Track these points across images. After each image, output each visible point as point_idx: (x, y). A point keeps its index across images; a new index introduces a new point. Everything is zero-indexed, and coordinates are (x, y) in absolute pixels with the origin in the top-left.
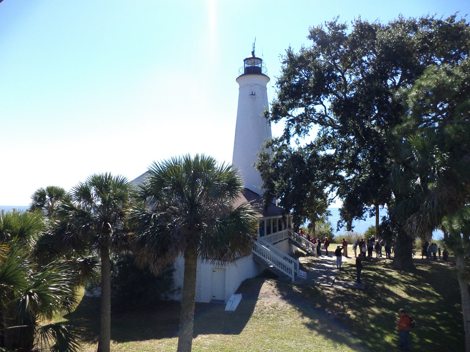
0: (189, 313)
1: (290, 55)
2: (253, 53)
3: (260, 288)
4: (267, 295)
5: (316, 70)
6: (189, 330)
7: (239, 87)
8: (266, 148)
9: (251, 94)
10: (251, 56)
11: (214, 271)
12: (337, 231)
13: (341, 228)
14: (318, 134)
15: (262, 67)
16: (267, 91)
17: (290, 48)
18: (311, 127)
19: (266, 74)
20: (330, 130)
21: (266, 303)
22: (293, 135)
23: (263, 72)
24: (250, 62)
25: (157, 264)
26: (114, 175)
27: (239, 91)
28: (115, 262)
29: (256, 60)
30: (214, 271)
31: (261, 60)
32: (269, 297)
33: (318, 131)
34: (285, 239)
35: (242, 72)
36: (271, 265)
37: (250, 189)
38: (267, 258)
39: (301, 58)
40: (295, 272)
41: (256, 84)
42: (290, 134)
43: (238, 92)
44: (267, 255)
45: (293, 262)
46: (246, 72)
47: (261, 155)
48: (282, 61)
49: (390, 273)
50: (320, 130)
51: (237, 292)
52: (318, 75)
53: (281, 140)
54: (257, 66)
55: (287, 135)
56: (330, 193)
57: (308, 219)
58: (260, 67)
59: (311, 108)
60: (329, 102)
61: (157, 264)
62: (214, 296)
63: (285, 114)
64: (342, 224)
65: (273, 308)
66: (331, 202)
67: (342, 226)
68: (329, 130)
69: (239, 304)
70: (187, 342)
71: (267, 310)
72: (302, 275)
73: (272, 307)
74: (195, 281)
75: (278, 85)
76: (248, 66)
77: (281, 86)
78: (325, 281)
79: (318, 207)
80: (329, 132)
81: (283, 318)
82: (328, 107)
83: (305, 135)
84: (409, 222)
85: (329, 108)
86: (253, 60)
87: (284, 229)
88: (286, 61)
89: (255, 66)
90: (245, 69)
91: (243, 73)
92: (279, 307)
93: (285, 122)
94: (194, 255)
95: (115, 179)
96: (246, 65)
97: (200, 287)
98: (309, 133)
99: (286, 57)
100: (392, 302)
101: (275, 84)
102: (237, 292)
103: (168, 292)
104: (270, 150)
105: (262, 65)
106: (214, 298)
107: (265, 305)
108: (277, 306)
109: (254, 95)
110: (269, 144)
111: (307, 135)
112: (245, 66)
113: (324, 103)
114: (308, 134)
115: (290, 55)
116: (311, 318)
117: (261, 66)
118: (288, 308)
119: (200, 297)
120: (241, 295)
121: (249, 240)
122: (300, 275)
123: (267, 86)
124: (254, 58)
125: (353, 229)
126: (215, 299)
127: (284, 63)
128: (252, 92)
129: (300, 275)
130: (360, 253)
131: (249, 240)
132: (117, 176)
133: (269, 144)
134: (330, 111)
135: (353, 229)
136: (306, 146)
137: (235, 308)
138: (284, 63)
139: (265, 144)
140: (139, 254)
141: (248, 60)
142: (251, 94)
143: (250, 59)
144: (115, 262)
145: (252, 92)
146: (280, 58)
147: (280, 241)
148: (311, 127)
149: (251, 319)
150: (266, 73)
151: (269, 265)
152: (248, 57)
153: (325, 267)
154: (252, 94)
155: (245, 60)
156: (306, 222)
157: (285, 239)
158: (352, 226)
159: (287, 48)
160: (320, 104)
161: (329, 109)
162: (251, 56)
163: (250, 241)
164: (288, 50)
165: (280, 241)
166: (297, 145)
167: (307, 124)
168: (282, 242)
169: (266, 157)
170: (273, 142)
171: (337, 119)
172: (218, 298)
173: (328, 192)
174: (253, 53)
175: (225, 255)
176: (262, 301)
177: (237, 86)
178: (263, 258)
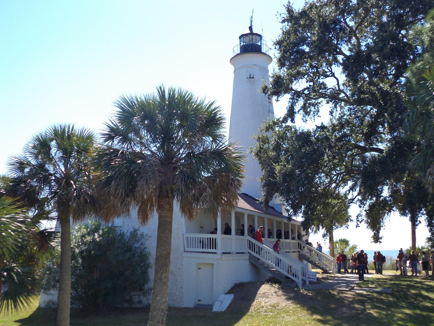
0: (164, 275)
1: (290, 10)
2: (251, 28)
3: (258, 288)
4: (265, 295)
5: (320, 20)
6: (163, 295)
8: (266, 131)
9: (249, 78)
10: (249, 32)
11: (199, 268)
12: (356, 227)
13: (361, 222)
14: (330, 113)
15: (262, 44)
17: (289, 3)
18: (321, 103)
19: (267, 53)
20: (346, 111)
21: (263, 303)
22: (299, 111)
23: (264, 50)
24: (247, 39)
25: (125, 205)
26: (78, 129)
27: (233, 75)
28: (77, 251)
29: (254, 36)
30: (199, 268)
31: (260, 36)
32: (268, 297)
33: (330, 110)
35: (238, 50)
37: (249, 195)
38: (266, 259)
39: (304, 14)
40: (302, 280)
41: (255, 65)
42: (295, 111)
43: (233, 75)
46: (243, 51)
47: (259, 138)
48: (281, 20)
49: (427, 283)
50: (332, 109)
51: (229, 292)
52: (322, 26)
53: (285, 120)
55: (291, 113)
56: (349, 192)
57: (323, 228)
59: (320, 82)
60: (342, 74)
61: (125, 205)
62: (199, 300)
63: (288, 90)
64: (361, 219)
65: (273, 307)
66: (352, 203)
67: (362, 221)
68: (345, 112)
69: (231, 304)
70: (161, 310)
71: (265, 308)
72: (310, 277)
73: (270, 306)
74: (170, 242)
75: (277, 47)
77: (280, 48)
79: (335, 210)
80: (345, 115)
81: (284, 316)
82: (341, 83)
83: (315, 117)
84: (430, 174)
85: (343, 83)
86: (251, 36)
88: (285, 19)
90: (241, 48)
91: (239, 52)
92: (280, 306)
93: (289, 100)
94: (169, 206)
95: (79, 134)
97: (182, 288)
98: (319, 114)
99: (285, 15)
100: (409, 263)
101: (273, 45)
102: (229, 292)
103: (142, 292)
104: (269, 134)
105: (262, 42)
107: (263, 304)
108: (278, 306)
109: (253, 78)
110: (269, 125)
111: (317, 116)
112: (240, 44)
113: (336, 75)
114: (318, 115)
115: (290, 10)
117: (261, 43)
118: (291, 308)
119: (182, 300)
121: (233, 182)
122: (308, 277)
123: (269, 68)
124: (252, 33)
125: (381, 240)
126: (202, 303)
127: (284, 21)
128: (250, 75)
129: (309, 278)
131: (233, 182)
132: (81, 129)
133: (269, 125)
134: (345, 86)
135: (381, 240)
136: (315, 128)
138: (284, 21)
139: (263, 126)
140: (105, 207)
142: (249, 77)
143: (246, 35)
144: (77, 251)
145: (250, 75)
146: (278, 16)
148: (321, 103)
149: (245, 318)
152: (245, 33)
153: (345, 280)
154: (250, 78)
155: (240, 37)
156: (320, 230)
158: (380, 236)
159: (286, 3)
160: (331, 76)
161: (343, 85)
162: (249, 32)
163: (234, 183)
164: (287, 5)
166: (304, 122)
168: (290, 253)
169: (265, 140)
170: (275, 123)
171: (350, 87)
172: (204, 302)
173: (348, 192)
174: (251, 28)
175: (204, 194)
176: (258, 302)
177: (232, 68)
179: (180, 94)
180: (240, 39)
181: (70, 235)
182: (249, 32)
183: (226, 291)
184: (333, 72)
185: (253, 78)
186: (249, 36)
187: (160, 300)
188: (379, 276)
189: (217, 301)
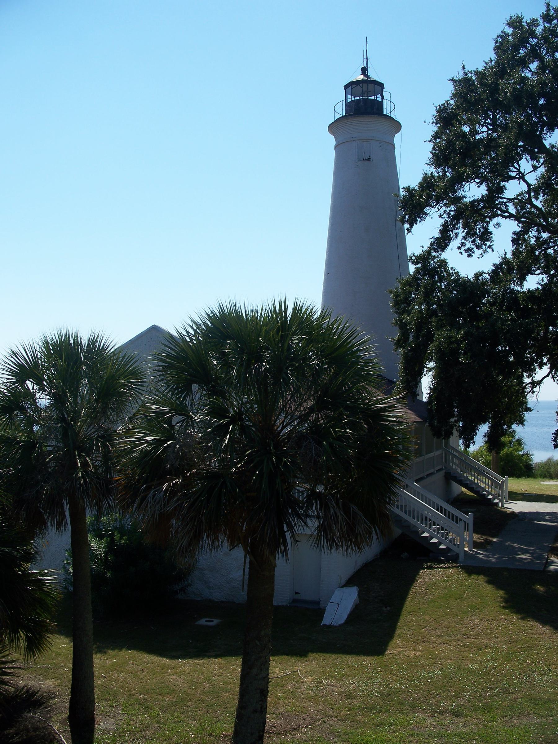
2: (364, 70)
7: (334, 143)
16: (395, 150)
19: (393, 116)
27: (334, 152)
29: (371, 86)
31: (381, 85)
34: (438, 471)
35: (342, 111)
36: (424, 532)
38: (414, 518)
43: (332, 154)
44: (414, 511)
45: (461, 520)
51: (349, 583)
54: (373, 98)
58: (380, 100)
62: (296, 593)
76: (353, 99)
78: (203, 518)
86: (364, 85)
87: (437, 450)
89: (369, 98)
90: (348, 105)
91: (344, 115)
96: (349, 97)
102: (349, 583)
106: (297, 597)
112: (346, 99)
116: (492, 540)
120: (275, 603)
123: (395, 142)
130: (310, 654)
137: (345, 616)
141: (353, 86)
147: (428, 475)
150: (393, 113)
151: (420, 533)
155: (346, 87)
157: (438, 471)
165: (428, 475)
167: (483, 121)
174: (364, 70)
177: (331, 140)
178: (406, 517)
179: (297, 311)
180: (345, 90)
181: (86, 520)
182: (361, 77)
183: (343, 582)
184: (523, 172)
185: (369, 159)
186: (361, 85)
187: (256, 675)
188: (405, 229)
189: (329, 603)
